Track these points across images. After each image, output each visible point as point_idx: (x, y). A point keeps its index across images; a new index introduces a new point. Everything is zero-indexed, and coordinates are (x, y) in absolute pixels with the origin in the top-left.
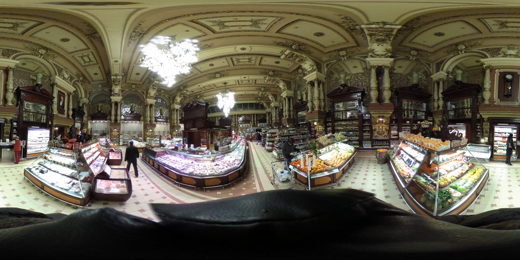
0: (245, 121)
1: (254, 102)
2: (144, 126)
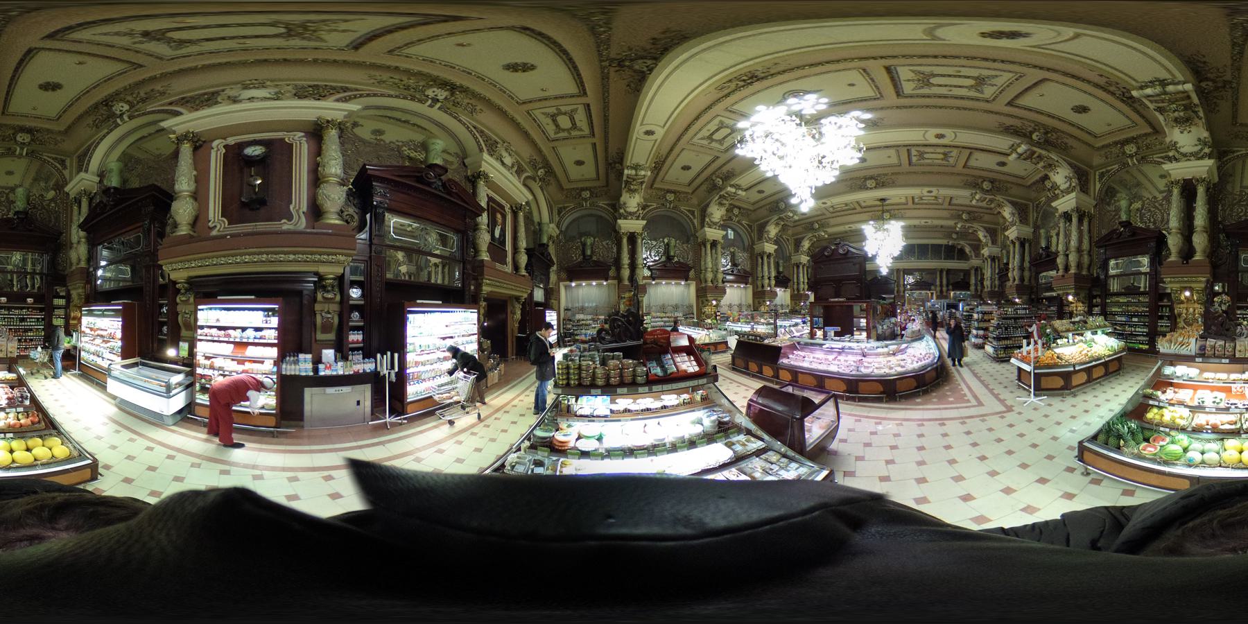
0: (919, 285)
2: (697, 291)
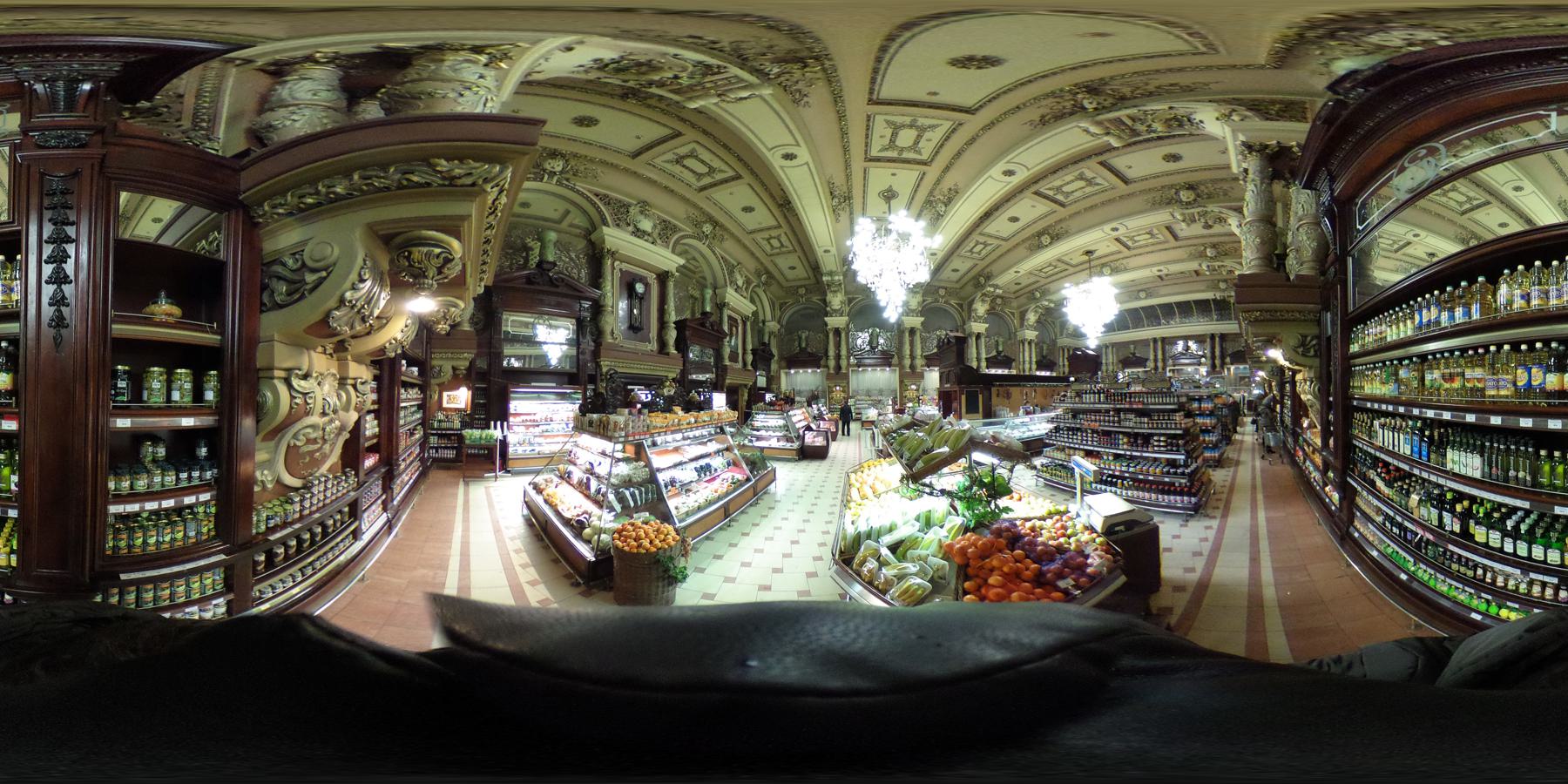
1: (1209, 295)
